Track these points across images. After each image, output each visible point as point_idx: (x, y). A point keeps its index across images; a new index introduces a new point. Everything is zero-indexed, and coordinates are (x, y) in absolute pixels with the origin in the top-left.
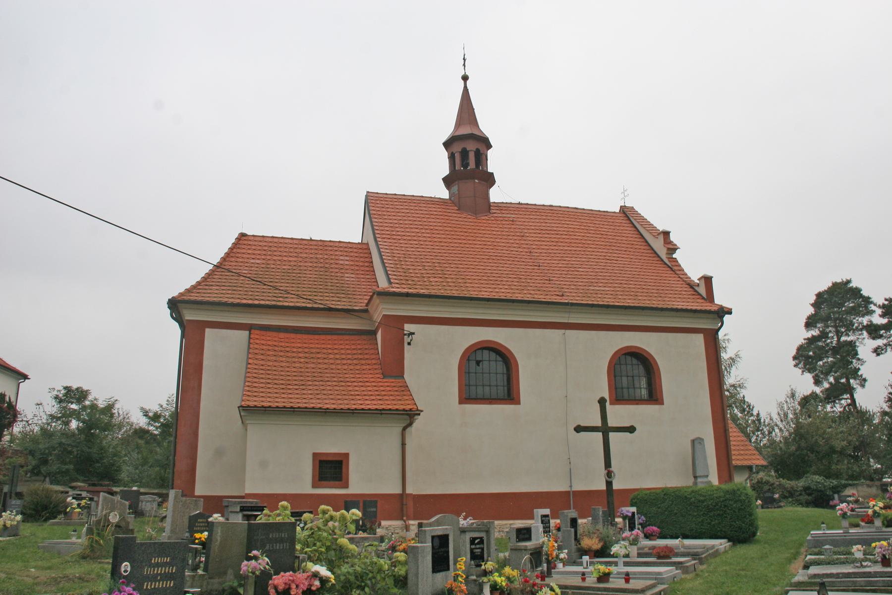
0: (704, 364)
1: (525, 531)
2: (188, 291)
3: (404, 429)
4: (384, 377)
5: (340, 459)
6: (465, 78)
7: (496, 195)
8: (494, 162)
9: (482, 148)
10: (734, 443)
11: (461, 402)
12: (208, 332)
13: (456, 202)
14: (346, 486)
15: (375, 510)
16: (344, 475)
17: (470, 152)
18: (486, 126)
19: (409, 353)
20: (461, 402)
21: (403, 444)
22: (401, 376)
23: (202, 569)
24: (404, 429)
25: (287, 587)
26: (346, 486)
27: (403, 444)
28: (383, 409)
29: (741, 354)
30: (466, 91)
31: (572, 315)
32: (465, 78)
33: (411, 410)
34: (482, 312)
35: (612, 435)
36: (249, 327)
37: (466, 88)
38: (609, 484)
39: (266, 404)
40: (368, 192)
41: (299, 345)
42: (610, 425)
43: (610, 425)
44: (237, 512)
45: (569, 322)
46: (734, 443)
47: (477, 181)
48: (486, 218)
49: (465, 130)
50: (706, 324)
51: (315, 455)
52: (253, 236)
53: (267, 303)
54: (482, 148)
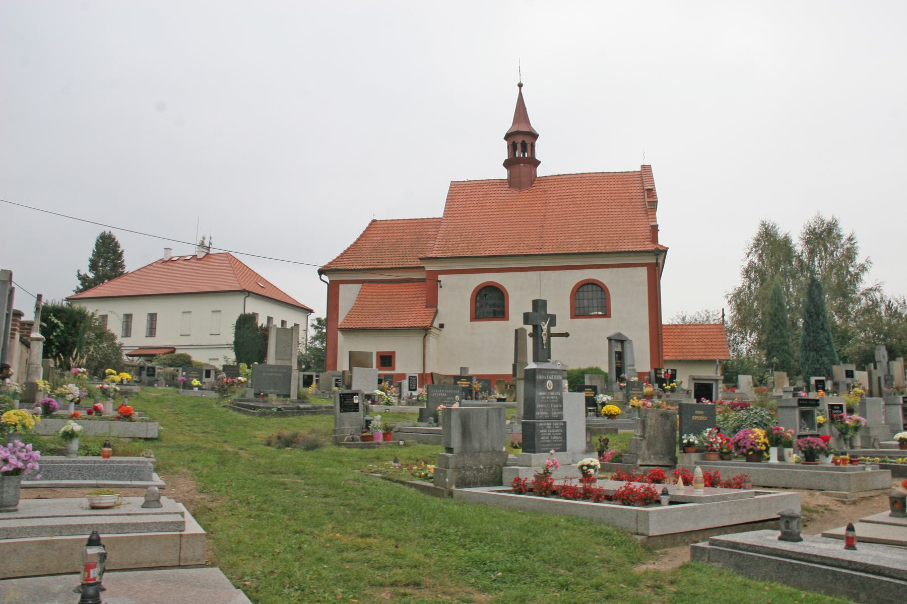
1: (838, 408)
2: (330, 263)
3: (425, 337)
4: (426, 307)
5: (390, 355)
6: (520, 85)
7: (541, 172)
8: (541, 150)
9: (528, 140)
10: (665, 337)
11: (471, 320)
12: (341, 286)
13: (512, 182)
14: (394, 369)
18: (536, 124)
19: (441, 293)
20: (471, 320)
21: (424, 346)
22: (437, 307)
24: (425, 337)
26: (394, 369)
27: (424, 346)
28: (411, 327)
29: (871, 259)
30: (520, 94)
31: (541, 261)
32: (520, 85)
33: (426, 326)
36: (363, 282)
37: (520, 95)
39: (350, 327)
40: (452, 182)
41: (388, 291)
44: (793, 407)
45: (541, 266)
46: (665, 337)
47: (522, 165)
48: (527, 191)
52: (381, 221)
53: (371, 267)
54: (528, 140)
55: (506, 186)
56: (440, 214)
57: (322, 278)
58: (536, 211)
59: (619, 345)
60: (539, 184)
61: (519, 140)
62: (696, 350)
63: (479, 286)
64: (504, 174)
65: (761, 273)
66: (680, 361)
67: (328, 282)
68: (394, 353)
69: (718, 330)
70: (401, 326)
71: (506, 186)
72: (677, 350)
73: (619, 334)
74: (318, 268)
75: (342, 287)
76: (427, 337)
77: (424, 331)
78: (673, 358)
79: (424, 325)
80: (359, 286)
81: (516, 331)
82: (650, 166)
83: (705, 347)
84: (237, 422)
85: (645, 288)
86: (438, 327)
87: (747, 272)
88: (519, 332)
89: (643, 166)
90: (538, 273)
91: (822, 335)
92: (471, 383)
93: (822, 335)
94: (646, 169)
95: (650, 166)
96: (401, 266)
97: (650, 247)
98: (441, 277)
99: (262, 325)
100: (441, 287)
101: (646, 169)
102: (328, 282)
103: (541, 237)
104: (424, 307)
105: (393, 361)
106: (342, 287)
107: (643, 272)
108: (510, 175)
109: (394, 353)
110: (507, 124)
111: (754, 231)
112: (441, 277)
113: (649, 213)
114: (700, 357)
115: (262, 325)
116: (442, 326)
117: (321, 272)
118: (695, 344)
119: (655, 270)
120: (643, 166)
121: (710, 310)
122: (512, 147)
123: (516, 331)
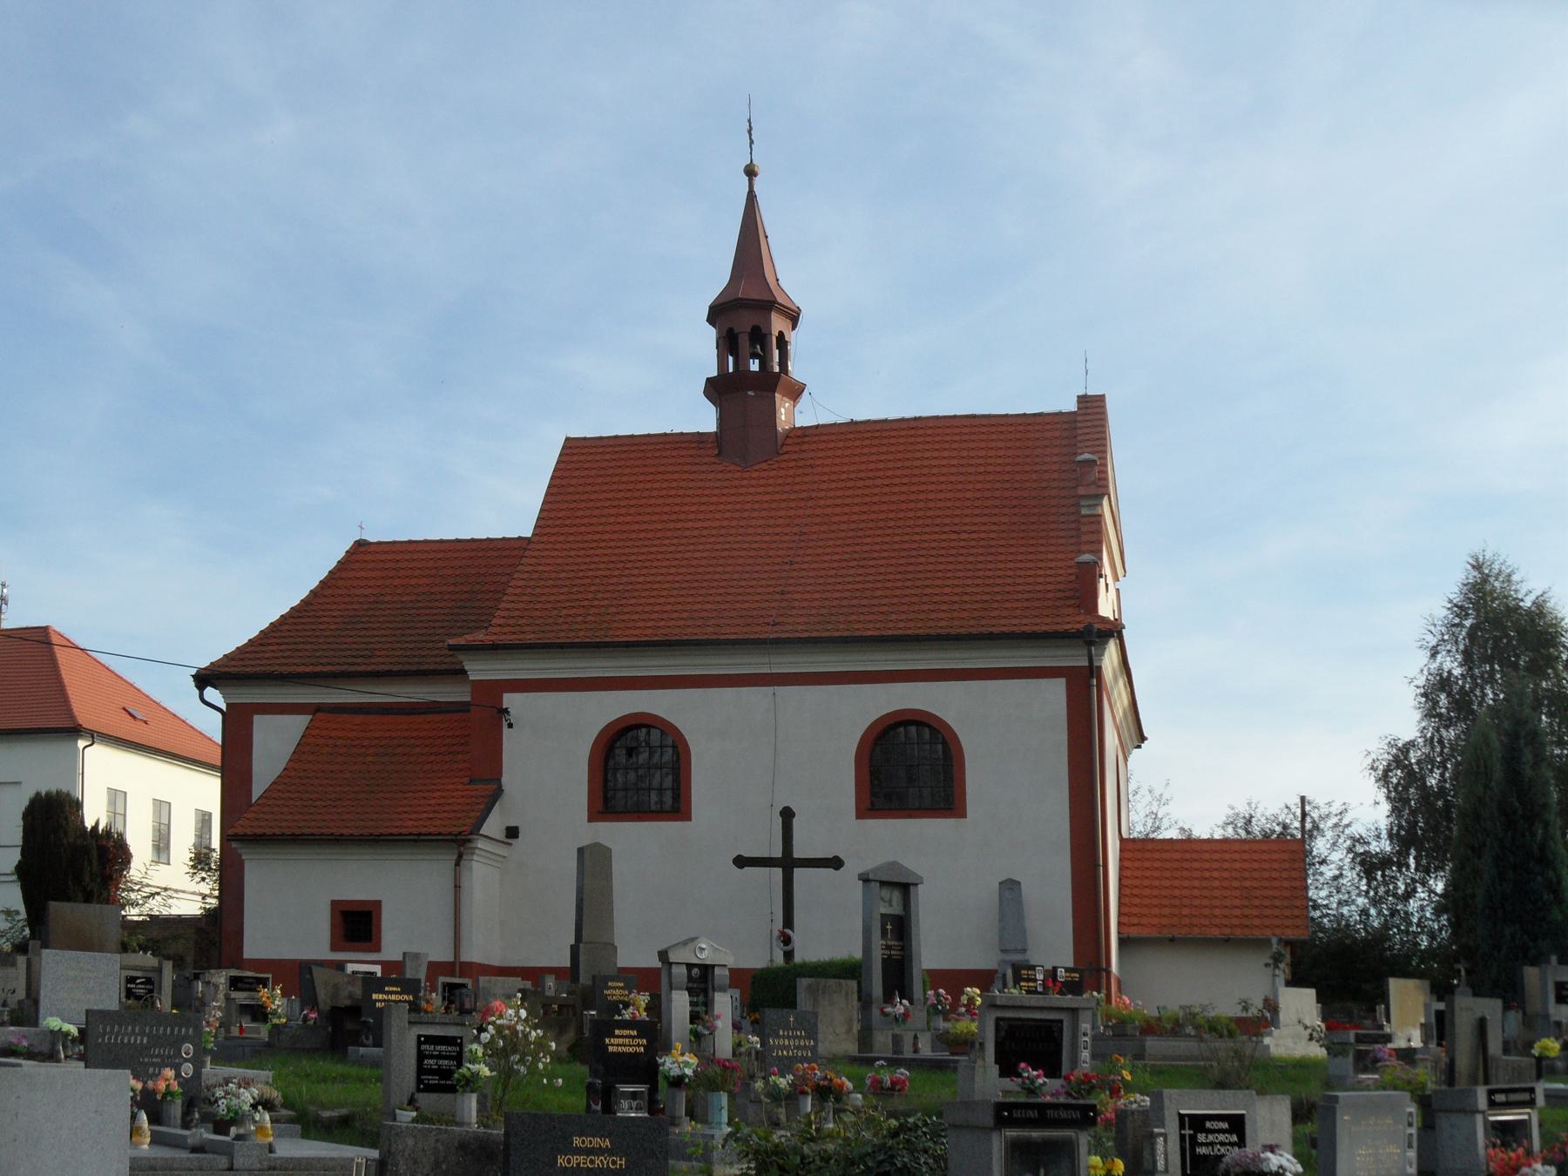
0: (1063, 737)
3: (457, 864)
6: (750, 172)
11: (591, 819)
15: (234, 995)
16: (374, 933)
17: (740, 336)
20: (591, 819)
21: (457, 887)
23: (1238, 1031)
24: (457, 864)
25: (1394, 1053)
27: (457, 887)
32: (750, 172)
34: (884, 658)
35: (778, 872)
36: (316, 709)
38: (789, 955)
42: (796, 855)
43: (796, 855)
47: (751, 393)
49: (747, 292)
50: (1075, 659)
51: (335, 904)
55: (710, 452)
56: (528, 533)
57: (206, 697)
58: (781, 521)
59: (896, 896)
60: (797, 448)
61: (744, 322)
62: (1217, 912)
63: (876, 722)
64: (704, 419)
65: (1462, 705)
66: (1172, 940)
67: (224, 707)
68: (378, 904)
69: (1285, 856)
70: (395, 831)
71: (710, 452)
72: (1166, 911)
73: (894, 865)
74: (194, 672)
75: (260, 722)
76: (462, 863)
77: (455, 845)
78: (1154, 933)
79: (456, 830)
80: (302, 721)
81: (581, 851)
82: (1101, 398)
83: (1246, 903)
84: (1197, 1027)
85: (1061, 737)
86: (501, 835)
87: (1429, 695)
88: (587, 855)
89: (1083, 400)
90: (769, 690)
91: (1539, 878)
92: (416, 997)
93: (1539, 878)
94: (1093, 407)
95: (1101, 398)
96: (414, 668)
97: (1074, 622)
98: (510, 700)
99: (97, 824)
100: (510, 726)
101: (1093, 407)
102: (224, 707)
103: (782, 593)
104: (466, 780)
105: (374, 928)
106: (260, 722)
107: (1055, 693)
108: (721, 421)
109: (378, 904)
110: (716, 277)
111: (1451, 583)
112: (510, 700)
113: (1084, 529)
114: (1227, 931)
115: (97, 824)
116: (512, 832)
117: (203, 679)
118: (1217, 893)
119: (1089, 686)
120: (1083, 400)
121: (1318, 797)
122: (728, 343)
123: (581, 851)
